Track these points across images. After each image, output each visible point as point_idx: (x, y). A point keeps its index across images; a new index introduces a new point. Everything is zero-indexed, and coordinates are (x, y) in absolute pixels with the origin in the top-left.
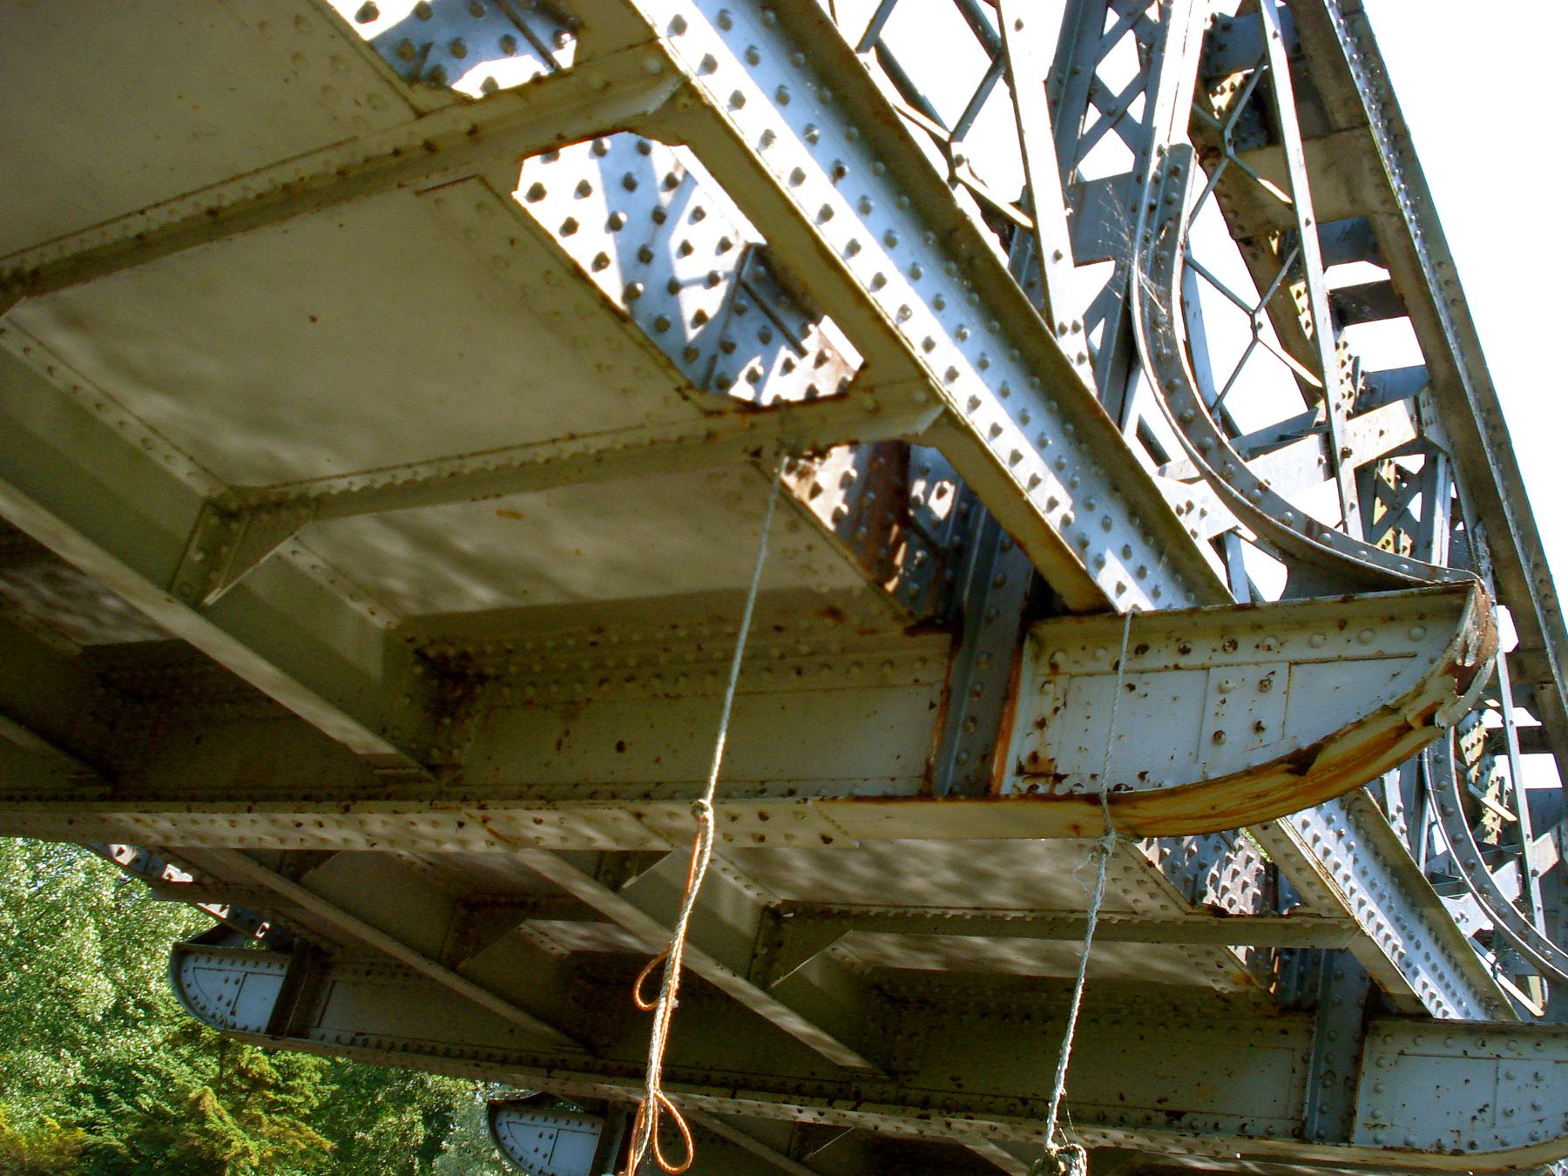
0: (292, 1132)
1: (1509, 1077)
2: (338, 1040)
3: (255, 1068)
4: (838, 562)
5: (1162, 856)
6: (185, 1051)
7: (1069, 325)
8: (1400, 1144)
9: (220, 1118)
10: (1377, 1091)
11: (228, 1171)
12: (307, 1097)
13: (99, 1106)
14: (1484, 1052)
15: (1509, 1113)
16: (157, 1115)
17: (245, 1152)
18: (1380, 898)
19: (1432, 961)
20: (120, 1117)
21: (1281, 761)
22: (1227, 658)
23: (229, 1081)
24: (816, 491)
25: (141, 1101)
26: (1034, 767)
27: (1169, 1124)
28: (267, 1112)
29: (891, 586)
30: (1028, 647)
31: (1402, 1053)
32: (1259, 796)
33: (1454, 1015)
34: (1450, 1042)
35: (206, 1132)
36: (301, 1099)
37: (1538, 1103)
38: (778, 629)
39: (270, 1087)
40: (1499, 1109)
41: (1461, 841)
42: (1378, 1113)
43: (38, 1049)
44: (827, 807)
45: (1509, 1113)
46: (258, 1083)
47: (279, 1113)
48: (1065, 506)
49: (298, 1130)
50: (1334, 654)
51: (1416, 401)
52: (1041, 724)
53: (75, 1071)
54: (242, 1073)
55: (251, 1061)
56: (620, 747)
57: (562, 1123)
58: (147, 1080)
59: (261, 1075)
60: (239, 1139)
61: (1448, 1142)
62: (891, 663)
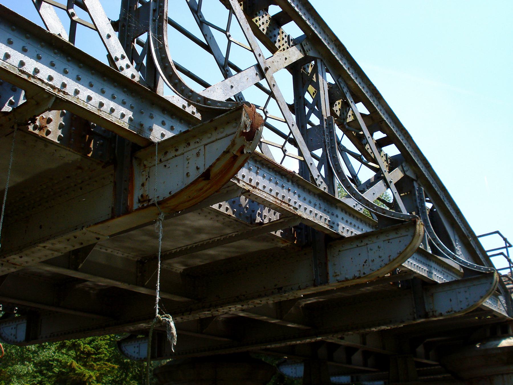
0: (104, 366)
1: (371, 250)
2: (46, 337)
3: (86, 350)
4: (68, 152)
5: (234, 212)
6: (64, 351)
7: (119, 57)
8: (344, 279)
9: (80, 368)
10: (334, 265)
11: (87, 384)
12: (105, 354)
13: (42, 376)
14: (363, 244)
15: (373, 261)
16: (61, 373)
17: (91, 377)
18: (315, 206)
19: (345, 219)
20: (50, 377)
21: (199, 177)
22: (188, 149)
23: (79, 356)
24: (48, 133)
25: (54, 370)
26: (143, 199)
27: (279, 292)
28: (94, 362)
29: (90, 155)
30: (134, 162)
31: (340, 251)
32: (201, 190)
33: (359, 233)
34: (352, 243)
35: (77, 374)
36: (103, 355)
37: (381, 255)
38: (68, 177)
39: (93, 354)
40: (370, 260)
41: (344, 180)
42: (336, 271)
43: (17, 364)
44: (89, 229)
45: (373, 261)
46: (89, 354)
47: (99, 361)
48: (129, 114)
49: (106, 364)
50: (215, 139)
51: (301, 44)
52: (143, 185)
53: (31, 367)
54: (83, 352)
55: (84, 348)
56: (41, 227)
57: (140, 342)
58: (55, 363)
59: (89, 351)
60: (88, 373)
61: (357, 275)
62: (104, 178)
